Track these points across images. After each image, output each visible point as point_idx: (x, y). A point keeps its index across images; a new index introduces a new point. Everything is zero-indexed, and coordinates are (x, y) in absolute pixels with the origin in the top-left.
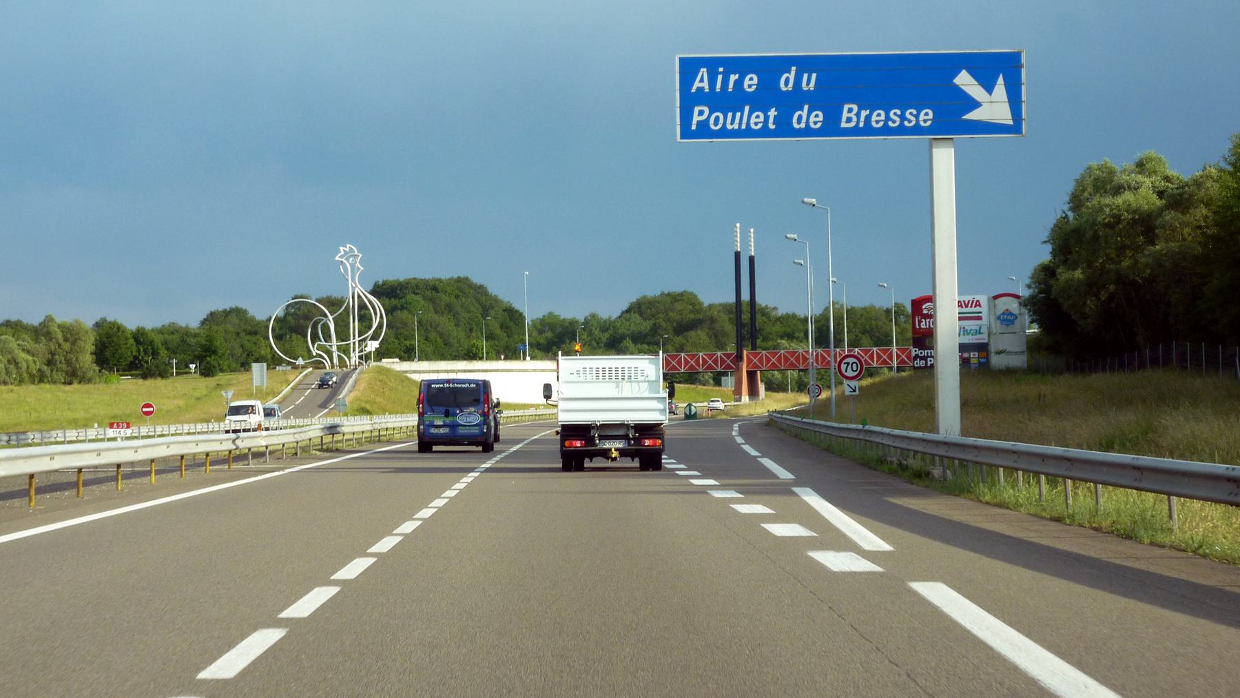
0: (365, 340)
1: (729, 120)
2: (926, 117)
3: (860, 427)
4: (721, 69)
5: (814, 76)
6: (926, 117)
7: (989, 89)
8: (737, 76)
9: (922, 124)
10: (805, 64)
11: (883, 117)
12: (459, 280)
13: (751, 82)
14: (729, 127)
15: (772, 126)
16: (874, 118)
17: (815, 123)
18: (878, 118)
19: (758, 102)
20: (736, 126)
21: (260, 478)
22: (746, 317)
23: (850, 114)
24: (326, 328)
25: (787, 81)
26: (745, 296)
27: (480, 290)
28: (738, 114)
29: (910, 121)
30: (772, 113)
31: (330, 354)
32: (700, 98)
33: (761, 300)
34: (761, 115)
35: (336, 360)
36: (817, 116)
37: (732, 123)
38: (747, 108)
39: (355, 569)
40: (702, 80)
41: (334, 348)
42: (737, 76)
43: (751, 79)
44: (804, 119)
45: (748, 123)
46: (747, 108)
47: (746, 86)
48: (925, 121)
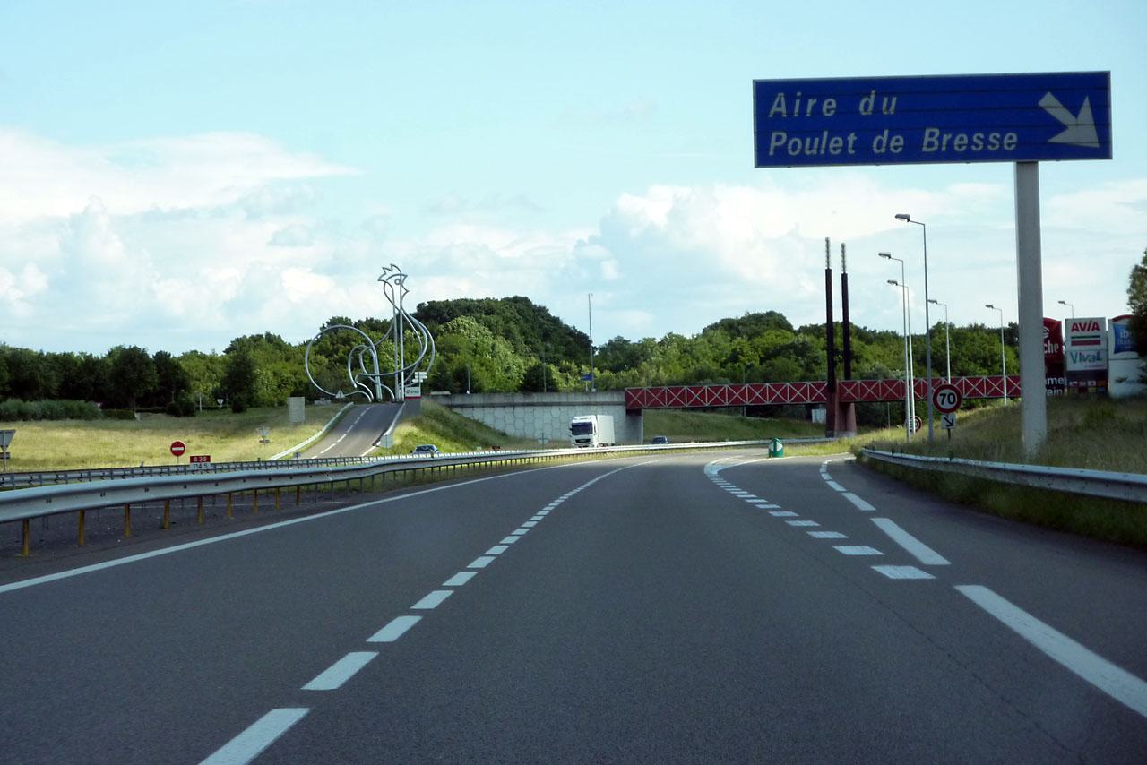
1: (807, 145)
4: (799, 94)
5: (894, 100)
7: (1075, 113)
8: (815, 101)
9: (1006, 147)
11: (966, 141)
12: (516, 300)
13: (829, 106)
15: (851, 151)
16: (957, 142)
21: (336, 512)
22: (838, 340)
25: (866, 105)
28: (817, 140)
30: (852, 138)
31: (373, 387)
33: (854, 319)
34: (840, 139)
35: (380, 395)
37: (810, 149)
38: (826, 134)
39: (433, 600)
42: (815, 101)
44: (884, 145)
45: (827, 148)
46: (826, 134)
47: (824, 110)
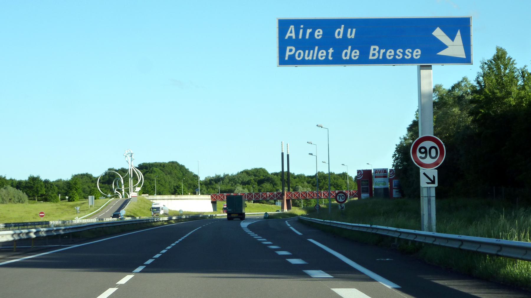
0: (135, 187)
2: (417, 53)
3: (369, 226)
4: (302, 26)
5: (354, 30)
6: (417, 53)
7: (453, 39)
8: (311, 30)
9: (415, 57)
10: (349, 23)
11: (393, 53)
12: (173, 163)
13: (319, 33)
14: (307, 58)
17: (355, 56)
18: (390, 54)
19: (323, 44)
20: (310, 58)
22: (285, 177)
23: (374, 51)
24: (120, 182)
25: (339, 34)
26: (286, 170)
27: (182, 167)
28: (312, 51)
29: (408, 56)
30: (331, 51)
32: (290, 42)
33: (291, 171)
36: (356, 53)
38: (317, 48)
40: (291, 32)
41: (123, 190)
43: (319, 32)
46: (317, 48)
47: (316, 36)
48: (416, 56)
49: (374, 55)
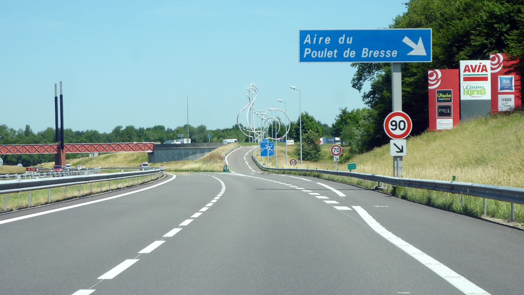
5: (351, 38)
7: (416, 43)
11: (378, 53)
13: (328, 40)
15: (335, 57)
25: (341, 40)
28: (323, 52)
30: (336, 51)
47: (326, 42)
49: (365, 54)
